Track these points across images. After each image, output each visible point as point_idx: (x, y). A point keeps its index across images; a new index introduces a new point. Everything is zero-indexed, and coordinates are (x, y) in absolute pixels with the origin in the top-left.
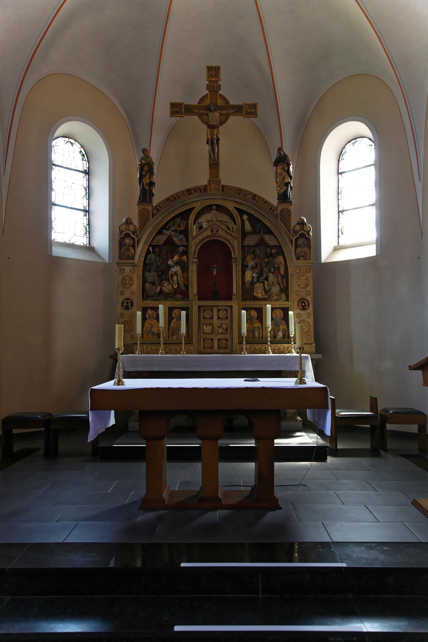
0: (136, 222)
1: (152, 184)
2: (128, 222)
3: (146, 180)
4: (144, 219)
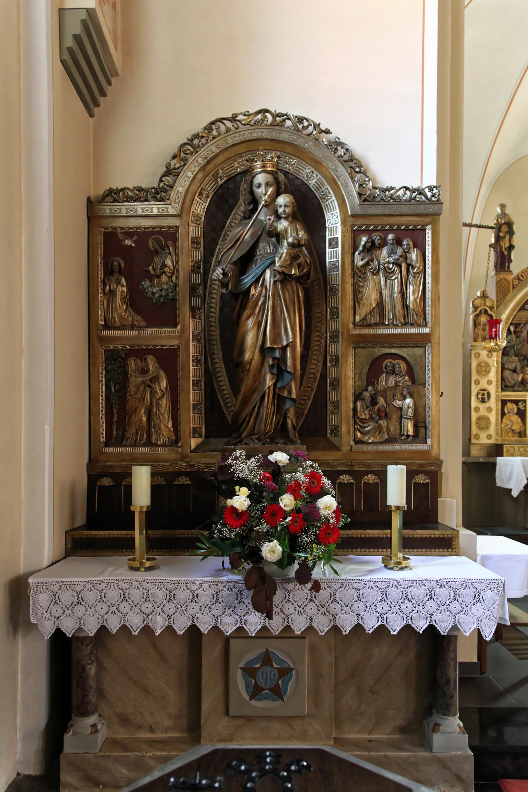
0: (492, 293)
1: (511, 247)
2: (484, 296)
3: (505, 244)
4: (504, 291)
